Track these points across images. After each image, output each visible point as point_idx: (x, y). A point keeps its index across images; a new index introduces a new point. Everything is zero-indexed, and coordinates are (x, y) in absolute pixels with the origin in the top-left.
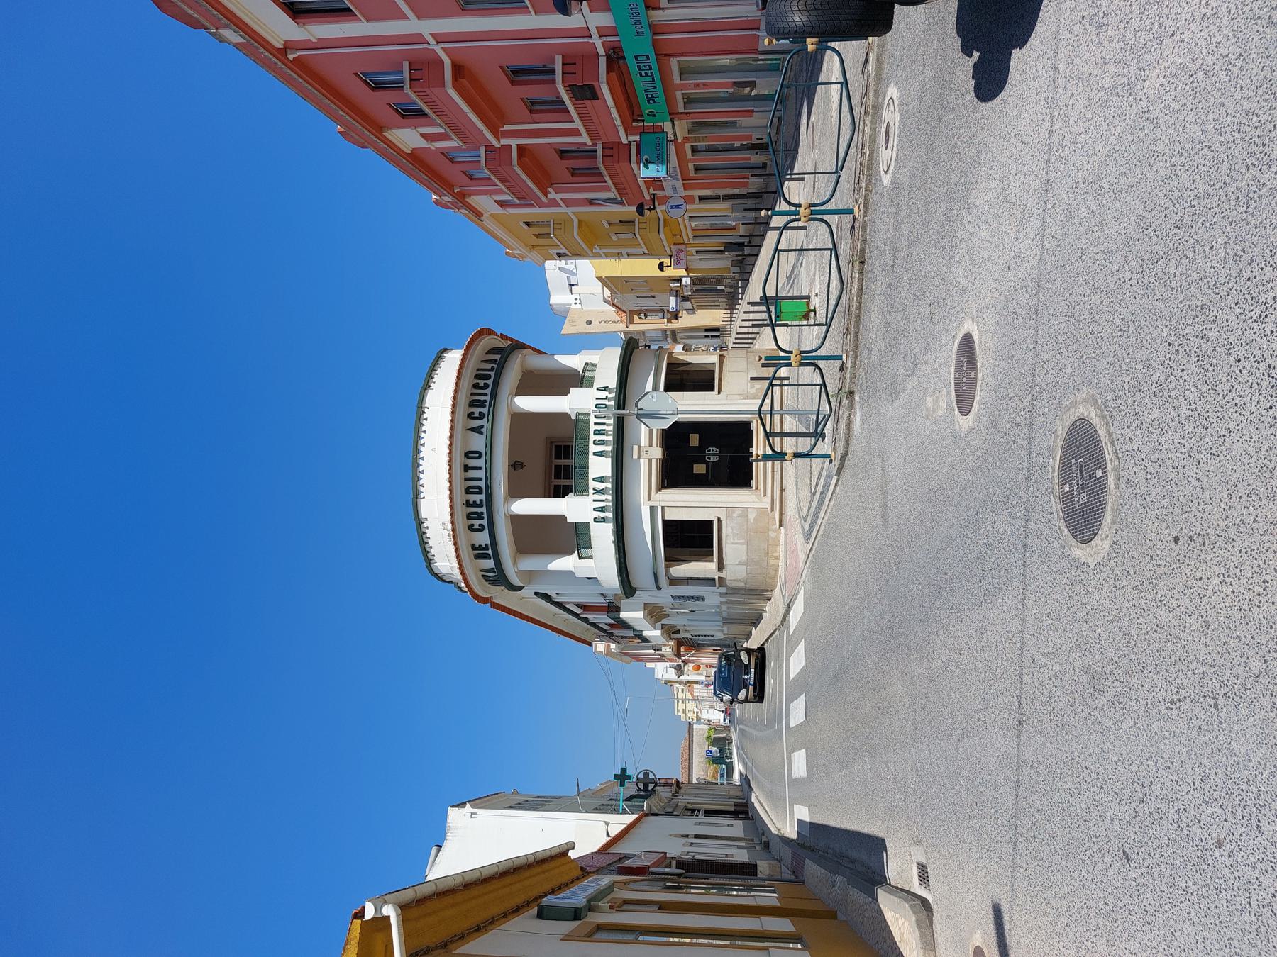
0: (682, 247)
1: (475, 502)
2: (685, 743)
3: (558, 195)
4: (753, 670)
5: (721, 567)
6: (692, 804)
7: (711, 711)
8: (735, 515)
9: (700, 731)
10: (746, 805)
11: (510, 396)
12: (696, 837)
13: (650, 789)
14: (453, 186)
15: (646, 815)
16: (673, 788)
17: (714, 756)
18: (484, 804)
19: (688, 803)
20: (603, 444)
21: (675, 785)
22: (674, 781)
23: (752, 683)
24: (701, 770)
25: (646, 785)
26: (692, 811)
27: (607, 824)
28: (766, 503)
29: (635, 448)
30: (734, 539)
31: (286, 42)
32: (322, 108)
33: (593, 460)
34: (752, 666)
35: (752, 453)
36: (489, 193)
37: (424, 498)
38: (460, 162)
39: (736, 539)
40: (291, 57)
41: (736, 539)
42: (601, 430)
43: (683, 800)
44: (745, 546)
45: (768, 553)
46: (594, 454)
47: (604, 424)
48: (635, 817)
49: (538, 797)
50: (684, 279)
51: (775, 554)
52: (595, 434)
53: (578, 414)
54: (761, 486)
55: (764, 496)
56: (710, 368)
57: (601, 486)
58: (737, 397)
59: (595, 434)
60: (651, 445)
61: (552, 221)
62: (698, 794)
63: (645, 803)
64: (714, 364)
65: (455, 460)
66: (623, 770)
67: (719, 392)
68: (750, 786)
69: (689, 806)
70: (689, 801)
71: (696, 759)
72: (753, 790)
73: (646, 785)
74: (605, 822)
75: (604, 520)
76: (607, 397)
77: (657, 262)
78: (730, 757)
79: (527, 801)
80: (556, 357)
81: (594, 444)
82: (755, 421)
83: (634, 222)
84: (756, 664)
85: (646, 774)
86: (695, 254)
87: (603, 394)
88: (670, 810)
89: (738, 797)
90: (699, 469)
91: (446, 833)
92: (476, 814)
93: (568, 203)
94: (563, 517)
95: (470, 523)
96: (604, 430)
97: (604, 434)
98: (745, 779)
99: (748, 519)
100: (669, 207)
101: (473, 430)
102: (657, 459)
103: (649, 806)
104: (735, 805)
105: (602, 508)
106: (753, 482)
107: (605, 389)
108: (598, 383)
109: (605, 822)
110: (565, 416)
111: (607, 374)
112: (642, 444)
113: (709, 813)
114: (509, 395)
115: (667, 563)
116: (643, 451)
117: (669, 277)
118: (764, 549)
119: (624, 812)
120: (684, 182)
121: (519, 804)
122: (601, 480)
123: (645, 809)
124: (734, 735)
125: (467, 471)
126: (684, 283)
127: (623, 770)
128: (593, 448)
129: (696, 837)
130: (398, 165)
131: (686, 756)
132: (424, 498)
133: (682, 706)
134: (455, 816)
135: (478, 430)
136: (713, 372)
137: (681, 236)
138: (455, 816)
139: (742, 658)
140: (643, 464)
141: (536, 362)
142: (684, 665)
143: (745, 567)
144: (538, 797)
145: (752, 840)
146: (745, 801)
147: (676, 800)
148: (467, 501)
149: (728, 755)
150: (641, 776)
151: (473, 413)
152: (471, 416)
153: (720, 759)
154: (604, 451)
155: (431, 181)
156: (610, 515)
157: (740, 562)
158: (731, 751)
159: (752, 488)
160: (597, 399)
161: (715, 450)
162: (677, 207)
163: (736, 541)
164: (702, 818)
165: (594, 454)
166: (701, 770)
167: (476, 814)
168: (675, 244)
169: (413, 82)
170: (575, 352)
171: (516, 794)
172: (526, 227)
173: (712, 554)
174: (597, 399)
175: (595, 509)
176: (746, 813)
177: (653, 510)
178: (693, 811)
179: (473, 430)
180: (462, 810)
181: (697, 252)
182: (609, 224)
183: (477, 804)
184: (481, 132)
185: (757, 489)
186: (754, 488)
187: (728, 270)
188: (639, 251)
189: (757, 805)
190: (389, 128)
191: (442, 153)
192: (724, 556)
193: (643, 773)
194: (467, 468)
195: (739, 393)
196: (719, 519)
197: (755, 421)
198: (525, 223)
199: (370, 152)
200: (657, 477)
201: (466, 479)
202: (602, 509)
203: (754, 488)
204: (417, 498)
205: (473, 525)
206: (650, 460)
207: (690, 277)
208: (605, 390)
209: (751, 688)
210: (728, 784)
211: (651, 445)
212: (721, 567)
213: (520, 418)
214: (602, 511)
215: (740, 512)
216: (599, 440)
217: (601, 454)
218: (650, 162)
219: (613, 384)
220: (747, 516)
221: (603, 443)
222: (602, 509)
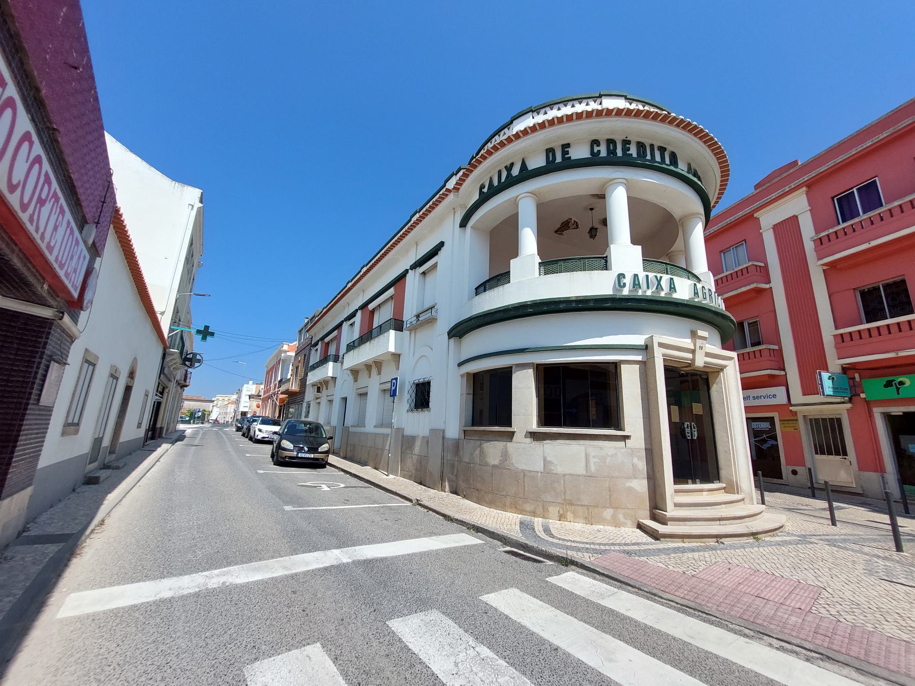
1: (629, 149)
2: (203, 398)
4: (312, 456)
6: (168, 393)
7: (218, 413)
8: (635, 460)
9: (208, 406)
10: (160, 436)
12: (128, 389)
13: (186, 362)
15: (165, 349)
16: (182, 382)
17: (195, 413)
18: (198, 217)
19: (169, 391)
21: (184, 384)
22: (187, 384)
23: (300, 455)
24: (188, 405)
26: (161, 390)
30: (594, 457)
34: (317, 456)
39: (596, 460)
41: (596, 460)
43: (172, 386)
44: (583, 472)
45: (572, 504)
48: (166, 335)
49: (193, 279)
51: (570, 515)
62: (175, 400)
63: (177, 351)
66: (212, 334)
68: (176, 441)
69: (166, 391)
70: (171, 391)
71: (192, 403)
72: (173, 445)
73: (190, 360)
74: (165, 311)
78: (194, 423)
79: (193, 266)
84: (317, 459)
85: (199, 361)
88: (166, 371)
89: (167, 430)
91: (179, 182)
92: (192, 209)
98: (181, 435)
99: (630, 478)
103: (173, 354)
104: (161, 428)
109: (165, 311)
113: (157, 406)
116: (702, 344)
119: (171, 330)
121: (192, 256)
122: (672, 288)
123: (171, 350)
124: (206, 425)
127: (212, 334)
129: (128, 389)
131: (195, 398)
133: (221, 398)
139: (324, 446)
142: (260, 399)
144: (193, 279)
145: (111, 452)
146: (164, 435)
147: (173, 381)
148: (629, 142)
149: (196, 422)
150: (198, 357)
152: (626, 143)
153: (193, 417)
156: (626, 292)
157: (551, 462)
158: (197, 423)
163: (592, 460)
164: (152, 399)
166: (188, 405)
167: (192, 209)
171: (198, 265)
176: (153, 438)
178: (162, 393)
180: (198, 200)
183: (200, 216)
184: (868, 241)
189: (160, 451)
193: (200, 358)
204: (533, 111)
205: (598, 145)
208: (671, 288)
210: (177, 422)
212: (534, 436)
215: (641, 468)
218: (832, 381)
220: (636, 478)
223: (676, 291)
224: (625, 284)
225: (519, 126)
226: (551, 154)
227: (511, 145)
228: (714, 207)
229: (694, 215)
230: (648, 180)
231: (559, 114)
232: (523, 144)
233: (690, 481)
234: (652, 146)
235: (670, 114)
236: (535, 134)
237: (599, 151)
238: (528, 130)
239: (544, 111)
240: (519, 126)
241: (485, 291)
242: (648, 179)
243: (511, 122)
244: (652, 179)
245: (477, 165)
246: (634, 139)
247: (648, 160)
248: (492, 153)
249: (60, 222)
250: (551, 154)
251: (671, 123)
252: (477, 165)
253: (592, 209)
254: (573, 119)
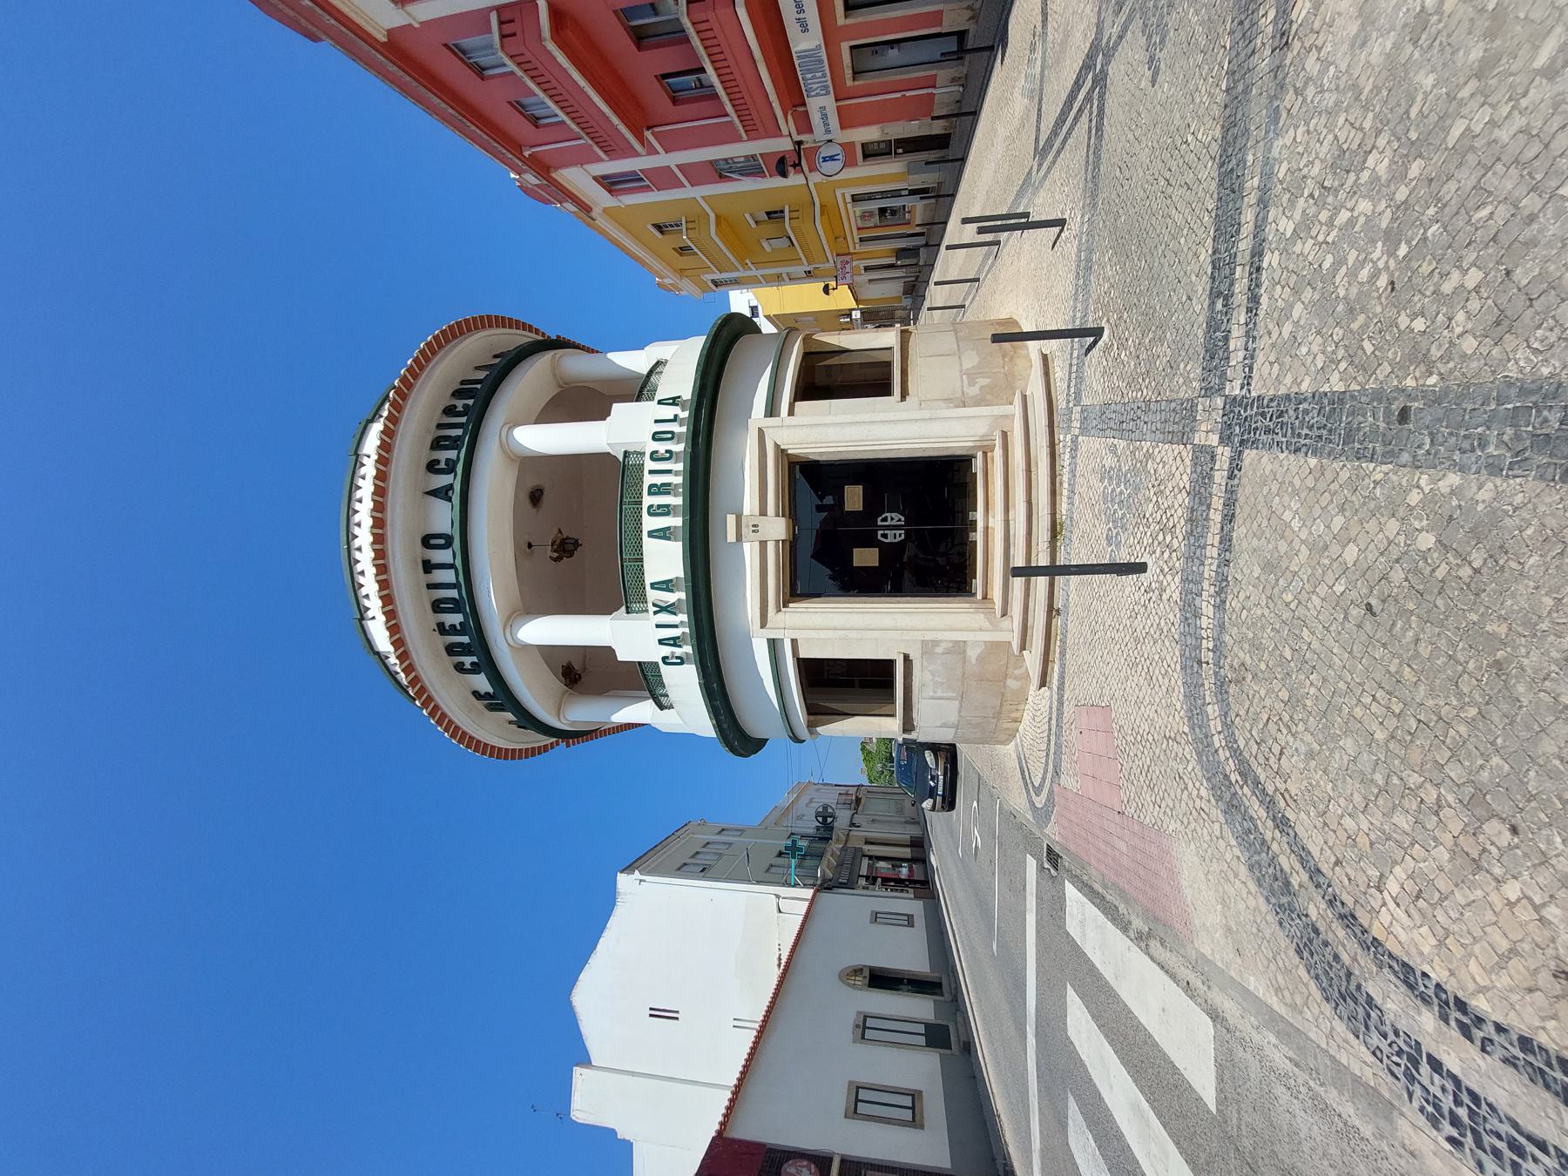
0: (848, 258)
3: (672, 155)
5: (908, 726)
11: (507, 427)
14: (521, 146)
20: (667, 514)
23: (940, 793)
25: (825, 819)
27: (778, 896)
28: (1010, 632)
29: (731, 519)
30: (935, 692)
31: (388, 31)
32: (419, 100)
33: (649, 545)
35: (974, 522)
36: (581, 162)
37: (374, 618)
38: (493, 77)
40: (526, 154)
42: (663, 485)
44: (956, 704)
45: (1000, 713)
46: (651, 534)
47: (669, 472)
50: (854, 313)
52: (650, 493)
53: (626, 453)
54: (996, 594)
55: (1003, 616)
56: (883, 357)
57: (671, 598)
58: (942, 404)
59: (650, 493)
60: (763, 512)
61: (684, 219)
64: (890, 348)
65: (394, 556)
67: (904, 395)
75: (682, 661)
76: (676, 416)
77: (823, 285)
80: (611, 356)
81: (650, 514)
82: (980, 455)
83: (782, 212)
86: (863, 272)
87: (669, 412)
90: (866, 557)
93: (695, 174)
94: (608, 652)
95: (456, 662)
96: (669, 484)
97: (669, 493)
99: (965, 657)
100: (821, 160)
101: (434, 493)
102: (777, 541)
105: (674, 639)
106: (978, 583)
107: (674, 401)
108: (664, 391)
110: (605, 458)
111: (681, 379)
112: (746, 511)
114: (505, 424)
115: (812, 718)
116: (747, 526)
117: (839, 310)
118: (994, 708)
120: (840, 104)
122: (666, 586)
125: (430, 572)
126: (854, 317)
128: (650, 523)
130: (370, 65)
131: (871, 627)
132: (374, 618)
134: (625, 882)
135: (443, 493)
136: (889, 365)
137: (845, 238)
138: (625, 882)
139: (928, 759)
140: (750, 551)
141: (577, 365)
143: (953, 730)
151: (438, 462)
152: (432, 467)
154: (669, 528)
155: (465, 120)
159: (974, 595)
160: (656, 421)
161: (895, 518)
162: (832, 158)
163: (939, 694)
165: (651, 534)
168: (838, 255)
169: (505, 40)
170: (639, 346)
172: (658, 234)
173: (891, 698)
174: (656, 421)
175: (661, 642)
177: (774, 645)
179: (434, 493)
181: (867, 269)
182: (757, 222)
185: (985, 597)
186: (979, 596)
187: (898, 299)
188: (799, 270)
190: (557, 168)
191: (445, 45)
192: (915, 715)
194: (428, 567)
195: (946, 397)
196: (906, 658)
197: (980, 455)
198: (653, 225)
199: (326, 48)
200: (777, 571)
201: (431, 586)
202: (675, 642)
203: (979, 596)
204: (362, 618)
206: (763, 544)
207: (861, 309)
208: (674, 404)
209: (939, 799)
211: (763, 512)
213: (531, 464)
214: (675, 645)
216: (659, 506)
217: (663, 534)
219: (686, 391)
220: (965, 652)
221: (665, 510)
222: (675, 642)
223: (679, 397)
224: (667, 451)
225: (382, 640)
226: (433, 542)
227: (408, 641)
228: (543, 334)
229: (554, 367)
230: (492, 597)
231: (371, 571)
232: (399, 556)
233: (972, 535)
234: (440, 426)
235: (395, 387)
236: (400, 614)
237: (473, 664)
238: (378, 547)
239: (356, 528)
240: (382, 640)
241: (667, 696)
242: (491, 599)
243: (378, 653)
244: (489, 596)
245: (433, 704)
246: (427, 455)
247: (465, 434)
248: (410, 664)
249: (981, 231)
250: (433, 542)
251: (410, 386)
252: (433, 704)
253: (530, 546)
254: (382, 535)
